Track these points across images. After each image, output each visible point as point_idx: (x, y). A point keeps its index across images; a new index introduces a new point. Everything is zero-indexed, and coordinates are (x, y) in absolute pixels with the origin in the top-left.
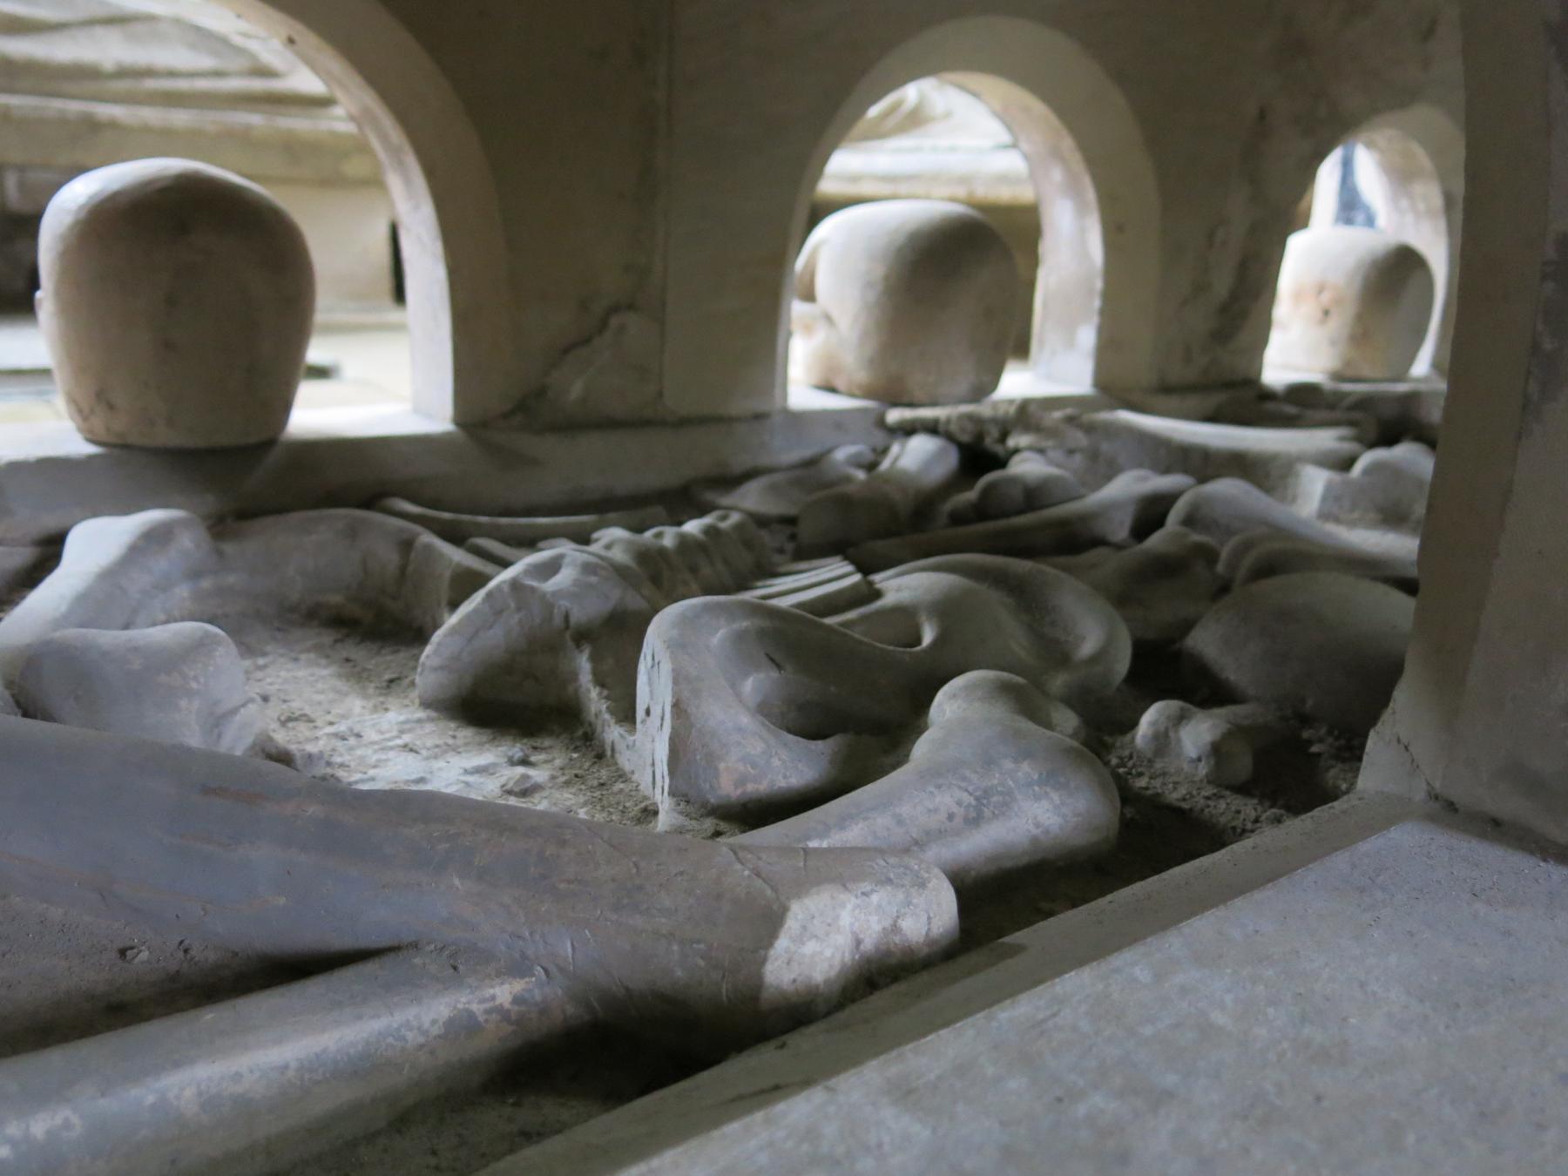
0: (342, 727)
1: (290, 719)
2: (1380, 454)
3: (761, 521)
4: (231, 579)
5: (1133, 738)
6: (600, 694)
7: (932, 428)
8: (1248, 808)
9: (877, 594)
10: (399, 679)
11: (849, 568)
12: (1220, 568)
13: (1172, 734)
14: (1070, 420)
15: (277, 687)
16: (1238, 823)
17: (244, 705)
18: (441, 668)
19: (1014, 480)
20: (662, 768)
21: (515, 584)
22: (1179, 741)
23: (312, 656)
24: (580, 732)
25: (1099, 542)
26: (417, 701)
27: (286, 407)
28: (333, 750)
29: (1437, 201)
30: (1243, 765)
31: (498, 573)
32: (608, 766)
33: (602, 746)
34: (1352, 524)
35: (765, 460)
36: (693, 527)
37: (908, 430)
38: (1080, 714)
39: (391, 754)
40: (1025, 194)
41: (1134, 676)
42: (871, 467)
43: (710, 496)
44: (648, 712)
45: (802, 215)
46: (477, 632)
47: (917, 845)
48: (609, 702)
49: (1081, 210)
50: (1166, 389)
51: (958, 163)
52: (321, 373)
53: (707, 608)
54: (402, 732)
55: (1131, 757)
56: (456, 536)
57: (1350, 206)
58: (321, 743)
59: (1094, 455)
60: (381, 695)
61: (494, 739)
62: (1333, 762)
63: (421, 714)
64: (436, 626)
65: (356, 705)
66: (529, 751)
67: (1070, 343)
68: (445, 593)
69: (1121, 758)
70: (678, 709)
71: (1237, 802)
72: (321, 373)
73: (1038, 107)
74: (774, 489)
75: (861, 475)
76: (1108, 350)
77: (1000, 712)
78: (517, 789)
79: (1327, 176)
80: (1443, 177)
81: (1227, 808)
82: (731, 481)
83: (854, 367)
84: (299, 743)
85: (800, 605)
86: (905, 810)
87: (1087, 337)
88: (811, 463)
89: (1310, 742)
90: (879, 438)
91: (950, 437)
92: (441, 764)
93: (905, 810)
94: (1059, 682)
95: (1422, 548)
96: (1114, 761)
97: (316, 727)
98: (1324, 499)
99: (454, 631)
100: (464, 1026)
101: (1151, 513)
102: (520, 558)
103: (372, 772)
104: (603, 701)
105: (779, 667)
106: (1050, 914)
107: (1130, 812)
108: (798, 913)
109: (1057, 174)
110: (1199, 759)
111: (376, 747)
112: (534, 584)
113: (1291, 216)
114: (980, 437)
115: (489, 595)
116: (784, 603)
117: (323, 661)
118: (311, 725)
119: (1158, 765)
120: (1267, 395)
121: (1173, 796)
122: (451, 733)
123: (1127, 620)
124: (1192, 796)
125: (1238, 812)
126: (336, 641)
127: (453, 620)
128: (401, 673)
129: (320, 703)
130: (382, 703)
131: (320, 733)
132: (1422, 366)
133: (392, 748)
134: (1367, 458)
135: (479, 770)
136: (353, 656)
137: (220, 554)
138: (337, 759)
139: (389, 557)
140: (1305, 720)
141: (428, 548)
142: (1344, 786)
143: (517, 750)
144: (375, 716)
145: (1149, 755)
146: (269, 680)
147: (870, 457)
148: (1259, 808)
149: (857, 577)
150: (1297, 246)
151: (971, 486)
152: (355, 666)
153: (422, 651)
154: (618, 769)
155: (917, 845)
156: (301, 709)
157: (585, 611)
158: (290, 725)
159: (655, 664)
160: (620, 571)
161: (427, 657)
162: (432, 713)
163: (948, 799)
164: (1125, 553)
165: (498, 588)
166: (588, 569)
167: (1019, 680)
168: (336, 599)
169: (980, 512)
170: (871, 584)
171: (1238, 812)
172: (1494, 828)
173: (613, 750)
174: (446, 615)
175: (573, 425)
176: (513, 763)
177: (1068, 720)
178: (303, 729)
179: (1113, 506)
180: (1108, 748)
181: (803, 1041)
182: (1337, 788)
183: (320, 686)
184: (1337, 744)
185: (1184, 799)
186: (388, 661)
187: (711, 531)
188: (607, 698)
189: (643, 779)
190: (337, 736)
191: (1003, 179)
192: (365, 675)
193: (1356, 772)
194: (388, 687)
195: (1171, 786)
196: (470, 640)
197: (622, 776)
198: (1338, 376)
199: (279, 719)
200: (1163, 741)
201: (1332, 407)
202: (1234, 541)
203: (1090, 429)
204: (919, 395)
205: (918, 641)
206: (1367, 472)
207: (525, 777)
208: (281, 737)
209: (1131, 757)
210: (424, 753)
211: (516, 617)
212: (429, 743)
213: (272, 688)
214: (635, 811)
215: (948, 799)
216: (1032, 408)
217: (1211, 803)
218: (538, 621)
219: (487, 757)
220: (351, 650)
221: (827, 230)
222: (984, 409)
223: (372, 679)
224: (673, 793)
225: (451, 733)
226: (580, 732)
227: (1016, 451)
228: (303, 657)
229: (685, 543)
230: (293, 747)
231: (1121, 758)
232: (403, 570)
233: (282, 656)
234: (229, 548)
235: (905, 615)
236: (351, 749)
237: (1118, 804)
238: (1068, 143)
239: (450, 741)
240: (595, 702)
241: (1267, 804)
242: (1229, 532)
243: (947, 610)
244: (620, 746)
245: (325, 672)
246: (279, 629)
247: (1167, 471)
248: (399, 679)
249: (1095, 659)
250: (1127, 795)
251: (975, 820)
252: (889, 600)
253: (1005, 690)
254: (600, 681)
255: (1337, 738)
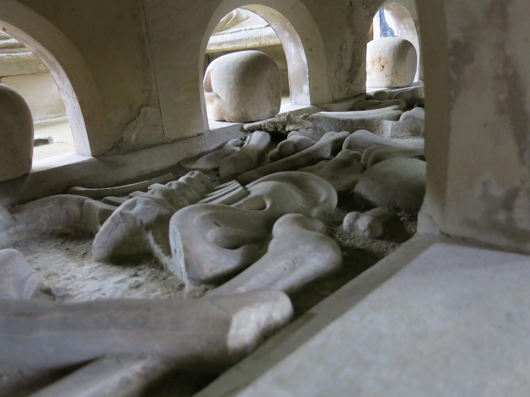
0: (68, 275)
1: (49, 276)
2: (408, 113)
3: (205, 172)
4: (20, 227)
5: (342, 227)
6: (158, 247)
7: (260, 129)
8: (383, 244)
9: (249, 193)
10: (86, 253)
11: (238, 185)
12: (362, 161)
13: (355, 223)
14: (305, 118)
15: (42, 264)
16: (381, 250)
17: (30, 275)
18: (101, 247)
19: (289, 142)
20: (184, 270)
21: (121, 214)
22: (357, 225)
23: (54, 250)
24: (153, 261)
25: (322, 159)
26: (94, 261)
27: (30, 161)
28: (66, 284)
29: (413, 24)
30: (380, 230)
31: (116, 209)
32: (165, 271)
33: (162, 264)
34: (402, 138)
35: (205, 149)
36: (182, 180)
37: (252, 130)
38: (324, 222)
39: (88, 282)
40: (277, 41)
41: (339, 205)
42: (241, 145)
43: (187, 166)
44: (175, 251)
45: (202, 60)
46: (111, 233)
47: (275, 281)
48: (162, 249)
49: (297, 46)
50: (335, 102)
51: (254, 34)
52: (45, 142)
53: (190, 210)
54: (90, 273)
55: (342, 234)
56: (98, 197)
57: (385, 30)
58: (62, 282)
59: (315, 128)
60: (81, 260)
61: (124, 269)
62: (408, 222)
63: (96, 265)
64: (97, 232)
65: (72, 265)
66: (136, 271)
67: (301, 91)
68: (98, 220)
69: (339, 235)
70: (185, 249)
71: (379, 243)
72: (45, 142)
73: (276, 13)
74: (209, 159)
75: (238, 149)
76: (314, 91)
77: (296, 228)
78: (134, 286)
79: (376, 20)
80: (412, 16)
81: (377, 246)
82: (195, 159)
83: (229, 112)
84: (54, 284)
85: (222, 202)
86: (269, 270)
87: (306, 88)
88: (221, 147)
89: (400, 217)
90: (242, 135)
91: (266, 131)
92: (106, 282)
93: (269, 270)
94: (315, 212)
95: (426, 143)
96: (337, 236)
97: (59, 277)
98: (392, 131)
99: (103, 233)
100: (126, 382)
101: (337, 146)
102: (123, 202)
103: (81, 290)
104: (159, 249)
105: (218, 225)
106: (325, 296)
107: (345, 253)
108: (236, 320)
109: (287, 35)
110: (365, 231)
111: (82, 280)
112: (128, 212)
113: (367, 37)
114: (276, 128)
115: (113, 219)
116: (215, 202)
117: (59, 251)
118: (57, 276)
119: (352, 235)
120: (369, 97)
121: (359, 245)
122: (108, 270)
123: (334, 185)
124: (365, 244)
125: (380, 246)
126: (62, 243)
127: (102, 229)
128: (87, 250)
129: (59, 267)
130: (82, 263)
131: (61, 279)
132: (416, 80)
133: (87, 279)
134: (404, 114)
135: (120, 282)
136: (69, 248)
137: (15, 219)
138: (68, 287)
139: (76, 210)
140: (397, 209)
141: (89, 204)
142: (413, 230)
143: (132, 271)
144: (80, 269)
145: (348, 232)
146: (39, 262)
147: (240, 142)
148: (387, 244)
149: (241, 188)
150: (370, 45)
151: (276, 147)
152: (70, 251)
153: (93, 241)
154: (169, 272)
155: (275, 281)
156: (53, 271)
157: (147, 218)
158: (49, 277)
159: (175, 234)
160: (158, 201)
161: (94, 244)
162: (100, 264)
163: (282, 264)
164: (330, 161)
165: (115, 215)
166: (147, 203)
167: (300, 215)
168: (60, 227)
169: (281, 155)
170: (246, 189)
171: (380, 246)
172: (464, 241)
173: (166, 265)
174: (99, 227)
175: (135, 149)
176: (132, 276)
177: (320, 225)
178: (54, 279)
179: (324, 146)
180: (335, 232)
181: (245, 365)
182: (411, 231)
183: (59, 260)
184: (409, 216)
185: (362, 245)
186: (81, 247)
187: (188, 179)
188: (161, 247)
189: (178, 274)
190: (69, 279)
191: (270, 36)
192: (74, 254)
193: (416, 224)
194: (83, 256)
195: (357, 241)
196: (109, 236)
197: (171, 274)
198: (390, 87)
199: (45, 276)
200: (352, 227)
201: (390, 98)
202: (365, 151)
203: (312, 120)
204: (253, 118)
205: (265, 207)
206: (405, 119)
207: (137, 281)
208: (47, 283)
209: (342, 234)
210: (100, 279)
211: (124, 225)
212: (101, 275)
213: (40, 265)
214: (177, 286)
215: (282, 264)
216: (292, 116)
217: (371, 245)
218: (132, 224)
219: (122, 276)
220: (68, 245)
221: (213, 66)
222: (276, 119)
223: (77, 255)
224: (189, 278)
225: (108, 270)
226: (153, 261)
227: (289, 131)
228: (51, 251)
229: (180, 186)
230: (51, 286)
231: (339, 235)
232: (82, 214)
233: (44, 252)
234: (17, 216)
235: (260, 198)
236: (73, 282)
237: (340, 252)
238: (288, 23)
239: (108, 273)
240: (157, 250)
241: (389, 242)
242: (363, 148)
243: (272, 194)
244: (168, 264)
245: (60, 255)
246: (40, 242)
247: (340, 131)
248: (86, 253)
249: (325, 201)
250: (343, 248)
251: (293, 268)
252: (253, 194)
253: (297, 220)
254: (157, 242)
255: (408, 214)
